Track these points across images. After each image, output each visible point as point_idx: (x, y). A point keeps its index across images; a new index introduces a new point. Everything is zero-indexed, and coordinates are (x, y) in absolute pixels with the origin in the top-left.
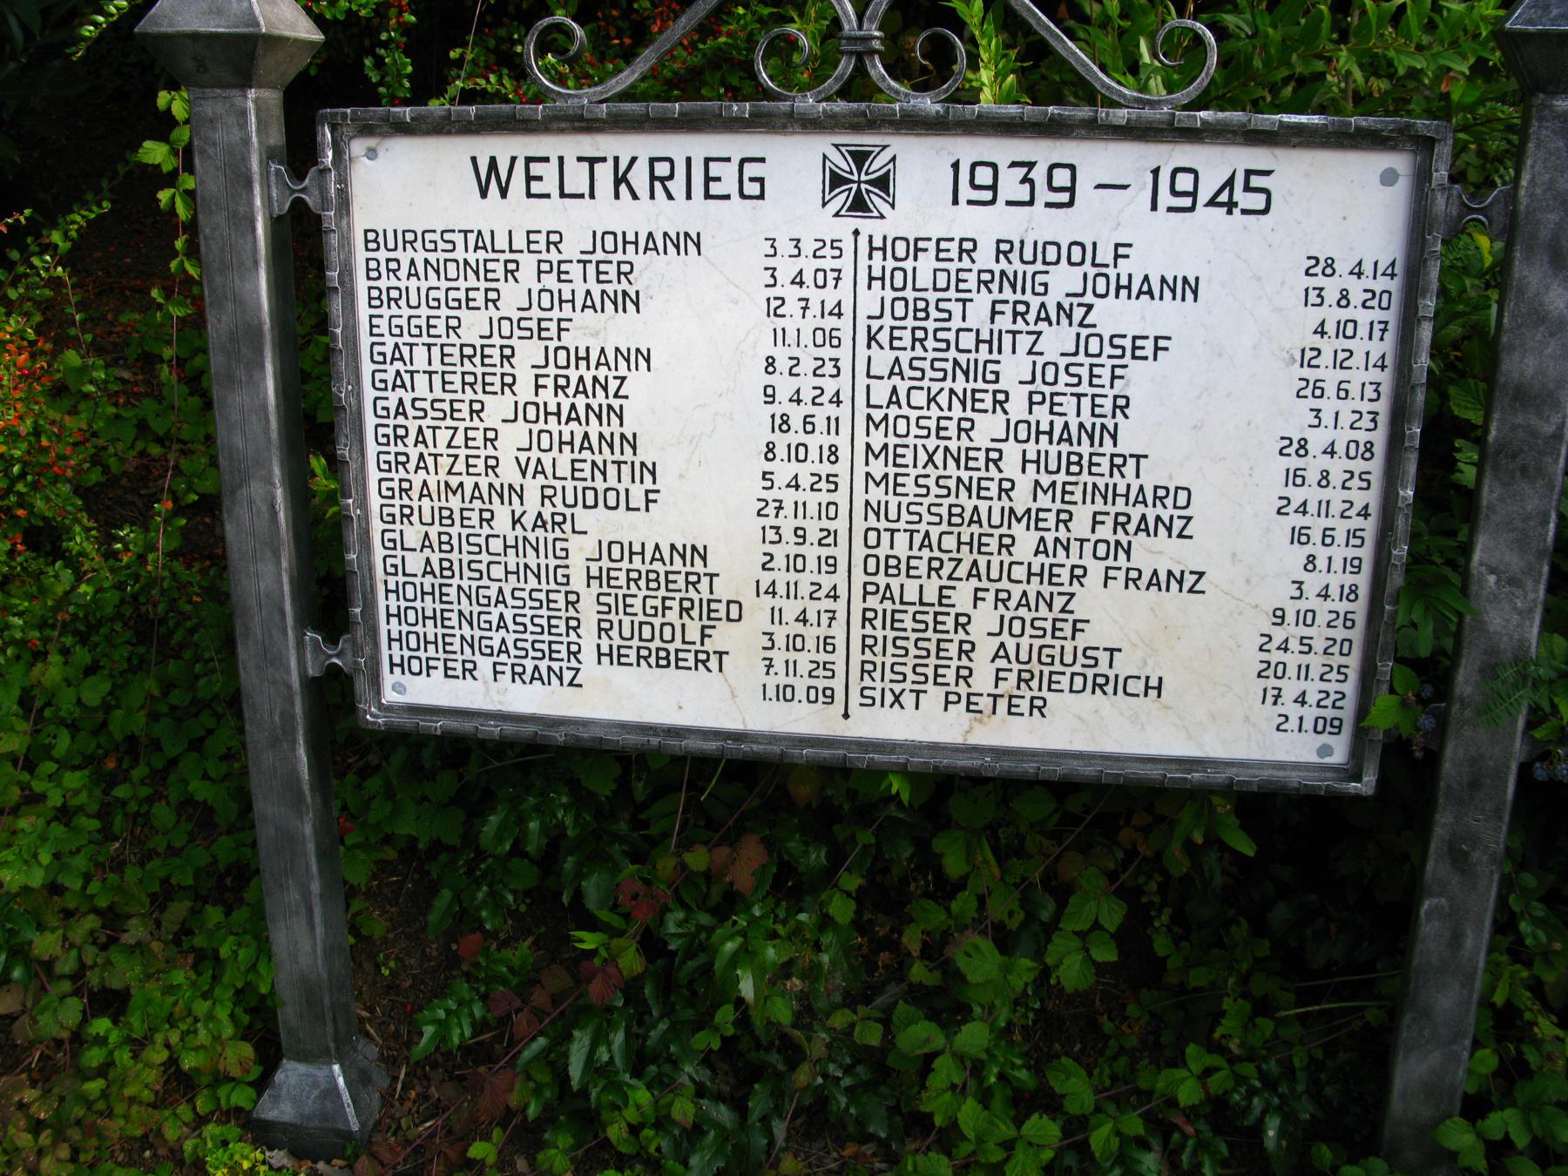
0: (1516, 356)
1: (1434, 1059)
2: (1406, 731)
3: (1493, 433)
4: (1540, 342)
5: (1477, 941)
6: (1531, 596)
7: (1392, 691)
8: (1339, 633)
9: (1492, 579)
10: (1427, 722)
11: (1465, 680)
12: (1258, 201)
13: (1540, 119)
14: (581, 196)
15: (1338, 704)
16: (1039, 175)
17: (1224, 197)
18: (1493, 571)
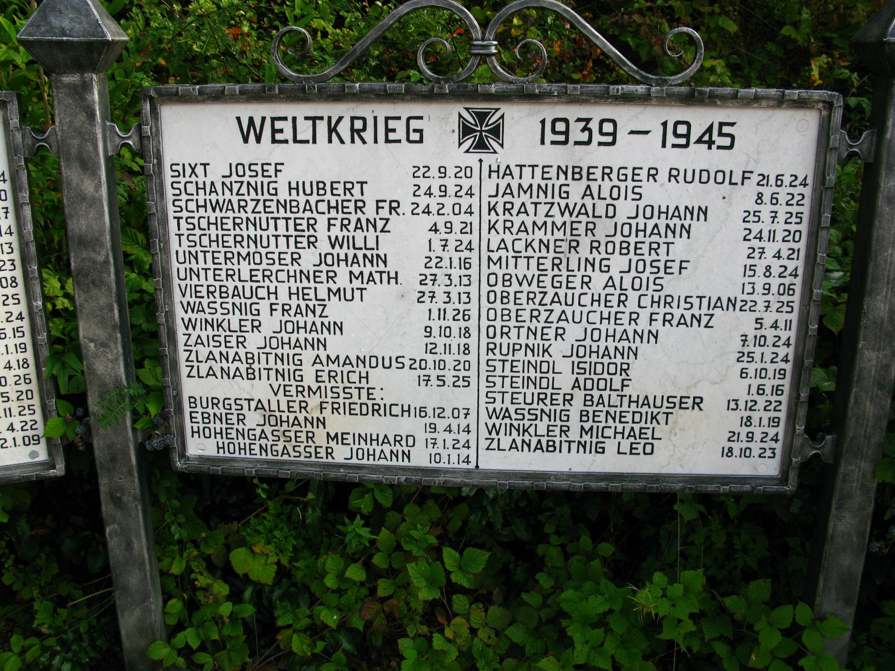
0: (75, 220)
1: (138, 612)
2: (71, 436)
3: (73, 264)
4: (86, 211)
5: (141, 545)
6: (115, 351)
7: (59, 415)
8: (24, 387)
9: (92, 345)
10: (80, 429)
11: (93, 403)
12: (727, 141)
13: (57, 88)
14: (307, 142)
15: (34, 427)
16: (594, 126)
17: (706, 138)
18: (91, 341)
